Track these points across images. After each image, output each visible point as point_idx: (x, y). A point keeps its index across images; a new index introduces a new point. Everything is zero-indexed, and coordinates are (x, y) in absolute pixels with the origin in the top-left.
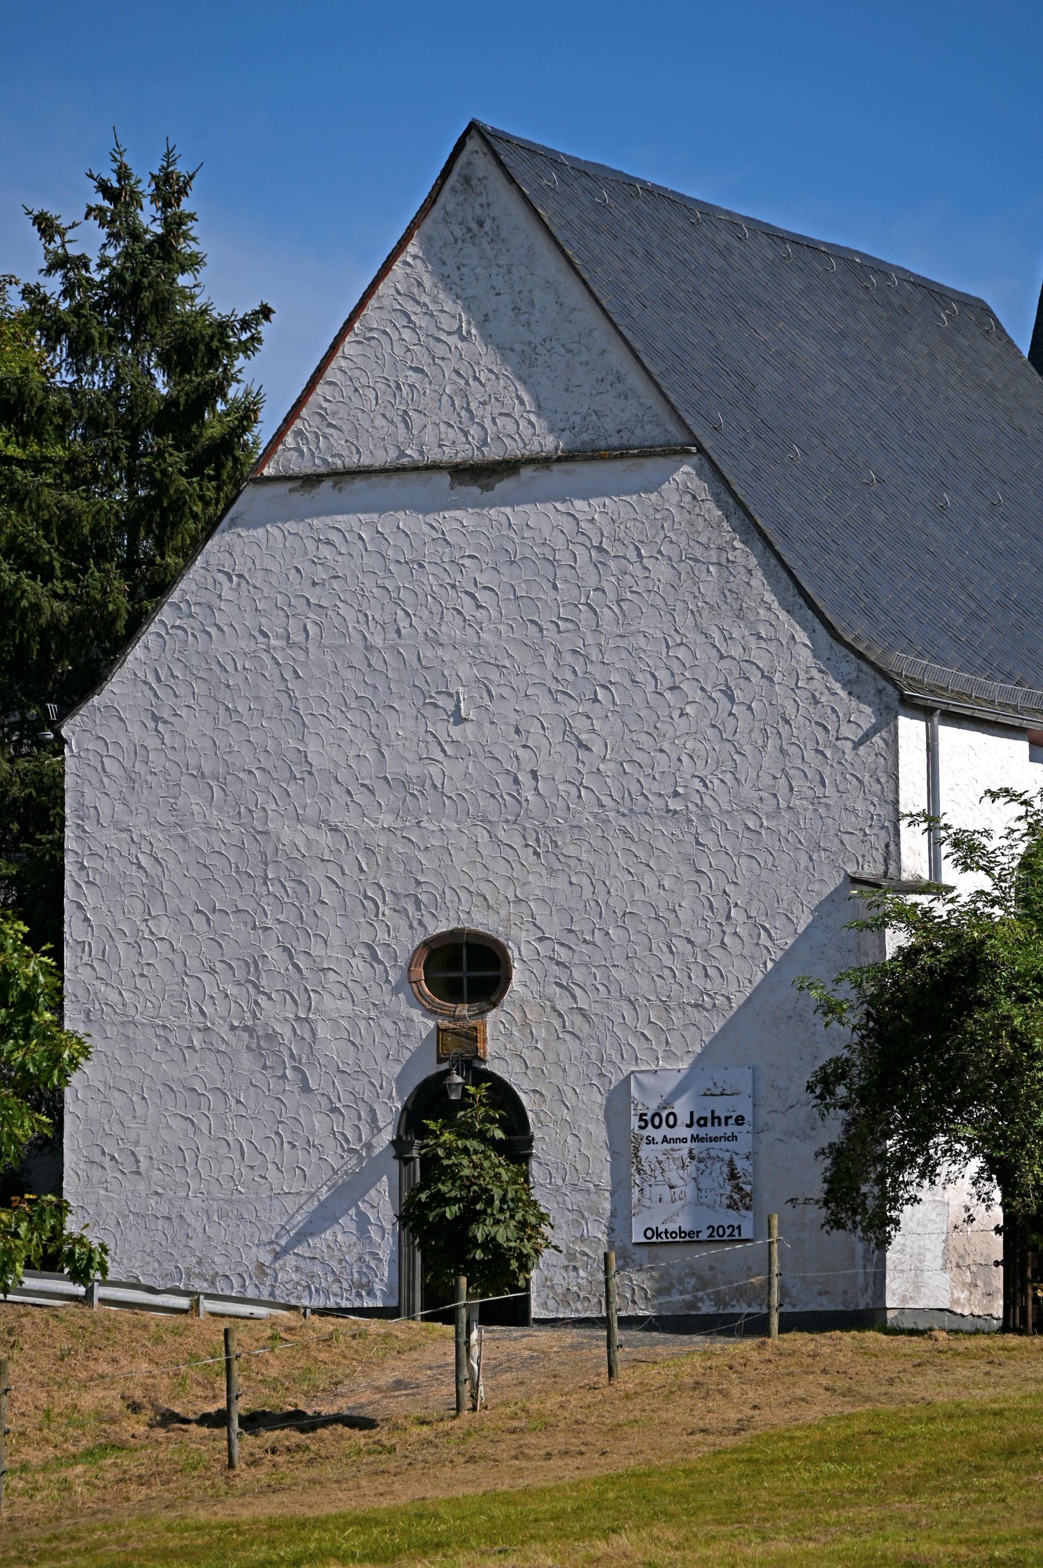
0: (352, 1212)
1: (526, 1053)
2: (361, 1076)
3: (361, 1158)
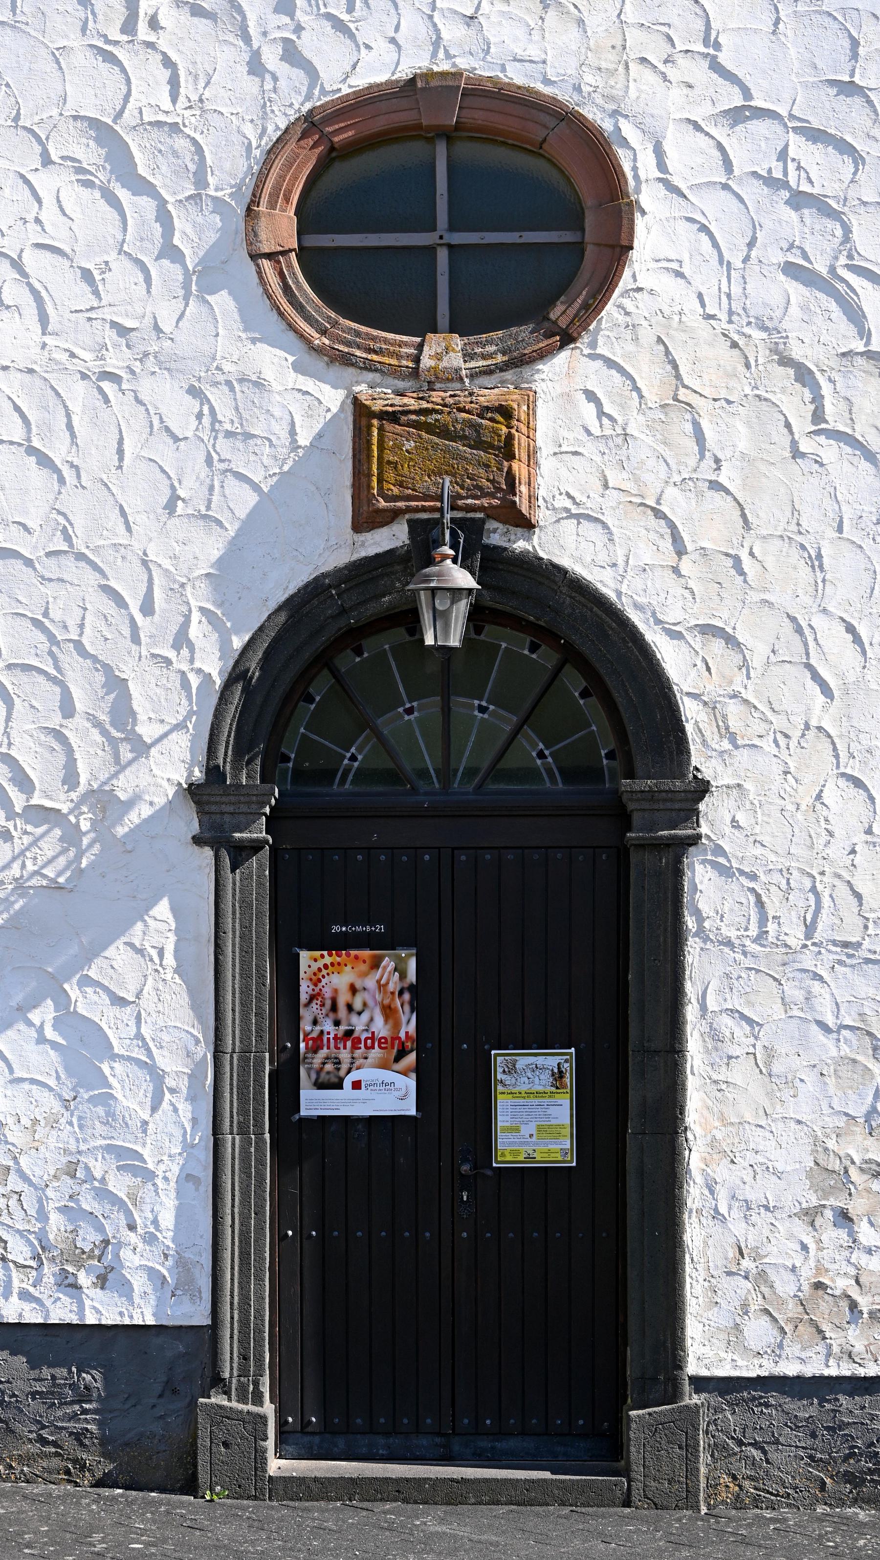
0: (44, 1014)
1: (676, 504)
2: (70, 569)
3: (71, 837)
